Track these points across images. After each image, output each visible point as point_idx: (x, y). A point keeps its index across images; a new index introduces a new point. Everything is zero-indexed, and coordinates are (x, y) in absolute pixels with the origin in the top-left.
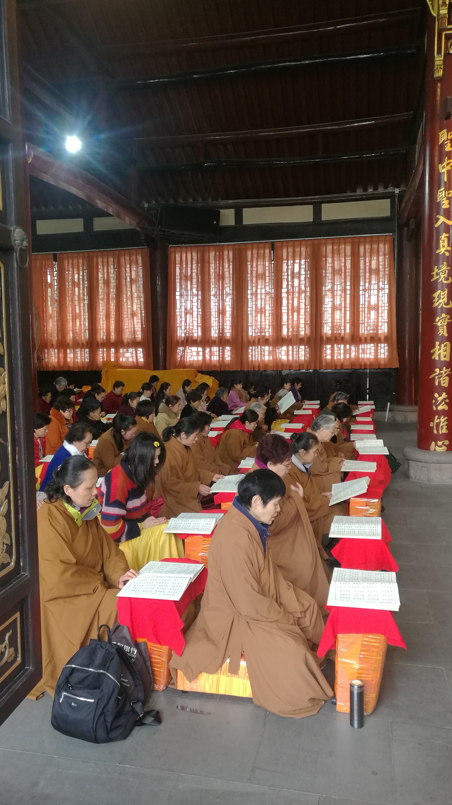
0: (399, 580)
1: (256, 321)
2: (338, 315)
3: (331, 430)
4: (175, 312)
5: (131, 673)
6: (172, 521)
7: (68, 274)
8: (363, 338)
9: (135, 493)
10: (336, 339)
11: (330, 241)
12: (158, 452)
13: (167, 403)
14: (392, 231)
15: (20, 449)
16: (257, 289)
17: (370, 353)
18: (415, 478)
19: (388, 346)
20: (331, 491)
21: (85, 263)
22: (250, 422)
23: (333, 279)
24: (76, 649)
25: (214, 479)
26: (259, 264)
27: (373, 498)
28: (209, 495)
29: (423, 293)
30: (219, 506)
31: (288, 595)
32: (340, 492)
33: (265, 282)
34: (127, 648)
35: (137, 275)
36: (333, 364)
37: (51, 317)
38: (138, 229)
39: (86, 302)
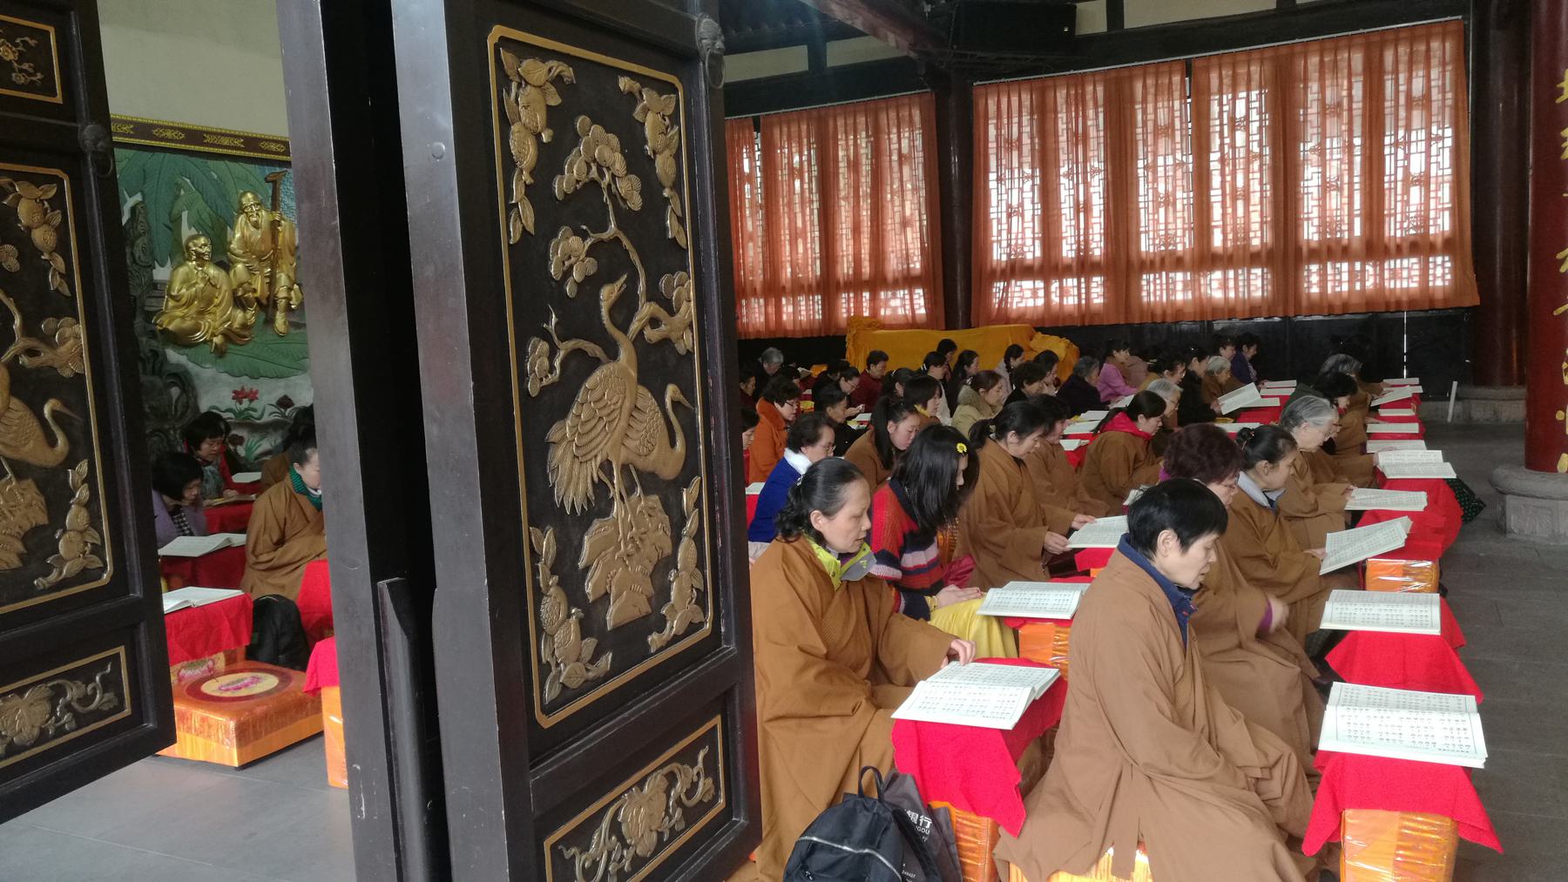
0: (1482, 709)
1: (1157, 222)
2: (1334, 200)
3: (1324, 428)
4: (987, 214)
5: (920, 860)
6: (993, 594)
7: (782, 153)
8: (1392, 247)
9: (919, 540)
10: (1331, 251)
11: (1316, 47)
12: (963, 464)
13: (976, 385)
14: (1463, 10)
15: (717, 419)
16: (1155, 155)
17: (1410, 277)
18: (1521, 531)
19: (1453, 260)
20: (1323, 545)
21: (813, 132)
22: (1148, 417)
23: (1323, 126)
24: (821, 807)
25: (1074, 525)
26: (1160, 107)
27: (1421, 558)
28: (1065, 554)
29: (1536, 142)
30: (1087, 573)
31: (1234, 733)
32: (1341, 548)
33: (1174, 142)
34: (913, 816)
35: (912, 147)
36: (1324, 304)
37: (751, 238)
38: (912, 55)
39: (816, 205)
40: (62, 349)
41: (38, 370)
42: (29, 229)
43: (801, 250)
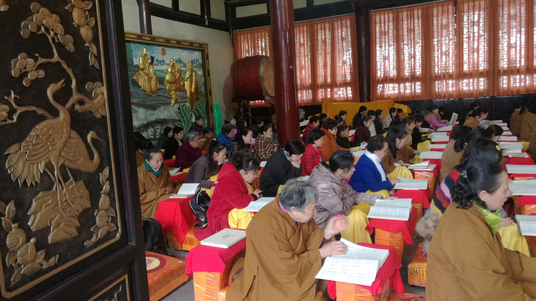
4: (376, 59)
10: (512, 71)
23: (509, 23)
40: (95, 101)
41: (84, 113)
42: (79, 26)
43: (304, 73)
